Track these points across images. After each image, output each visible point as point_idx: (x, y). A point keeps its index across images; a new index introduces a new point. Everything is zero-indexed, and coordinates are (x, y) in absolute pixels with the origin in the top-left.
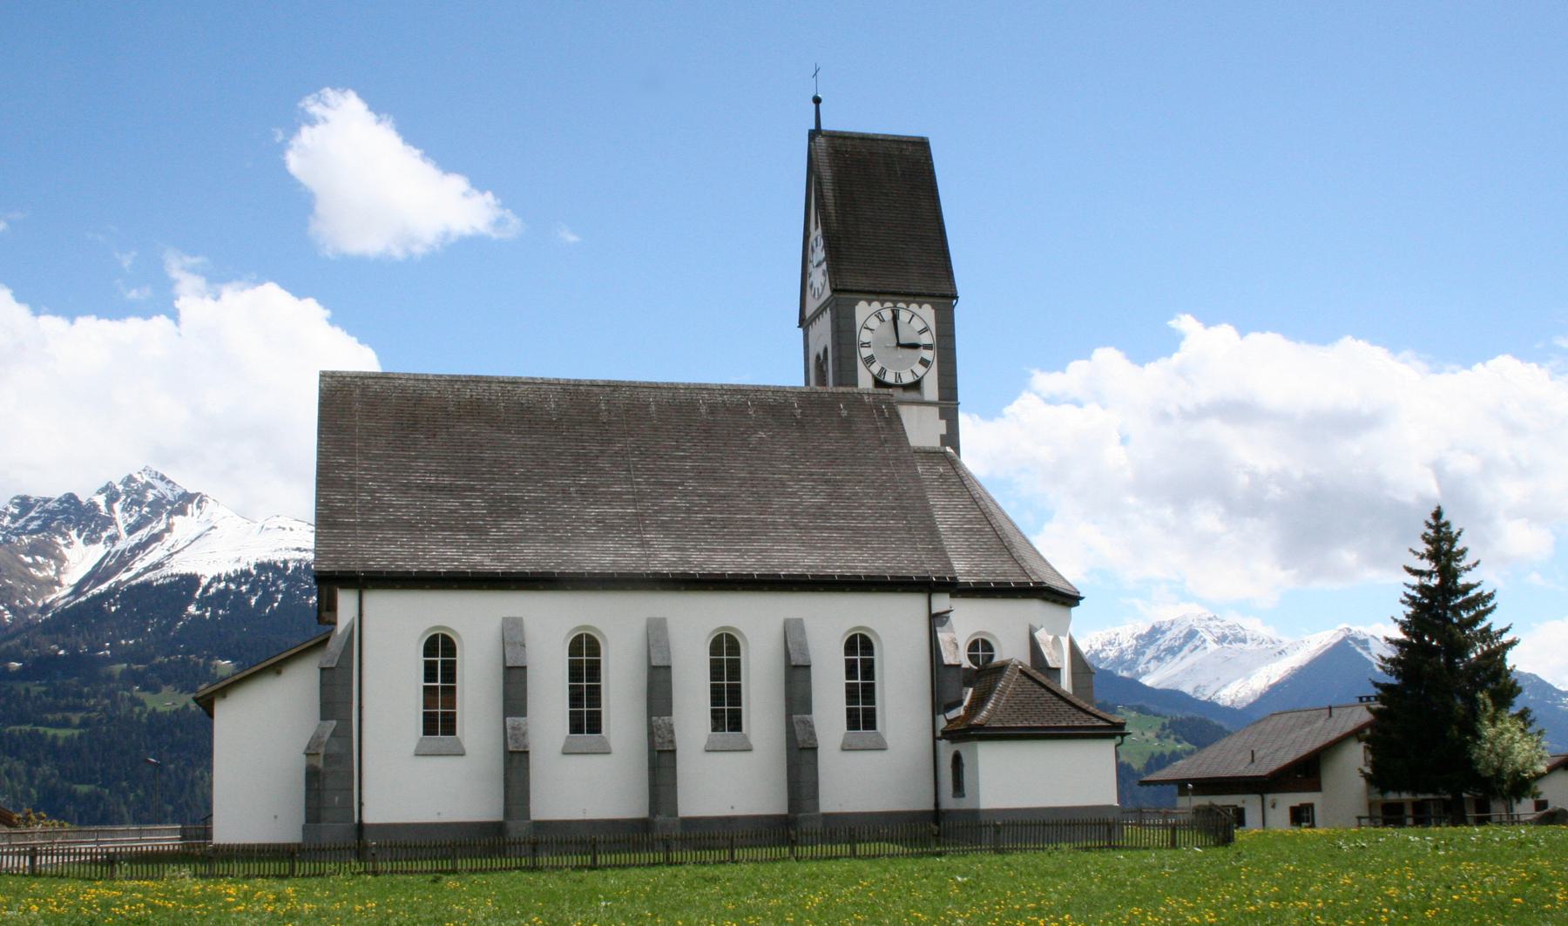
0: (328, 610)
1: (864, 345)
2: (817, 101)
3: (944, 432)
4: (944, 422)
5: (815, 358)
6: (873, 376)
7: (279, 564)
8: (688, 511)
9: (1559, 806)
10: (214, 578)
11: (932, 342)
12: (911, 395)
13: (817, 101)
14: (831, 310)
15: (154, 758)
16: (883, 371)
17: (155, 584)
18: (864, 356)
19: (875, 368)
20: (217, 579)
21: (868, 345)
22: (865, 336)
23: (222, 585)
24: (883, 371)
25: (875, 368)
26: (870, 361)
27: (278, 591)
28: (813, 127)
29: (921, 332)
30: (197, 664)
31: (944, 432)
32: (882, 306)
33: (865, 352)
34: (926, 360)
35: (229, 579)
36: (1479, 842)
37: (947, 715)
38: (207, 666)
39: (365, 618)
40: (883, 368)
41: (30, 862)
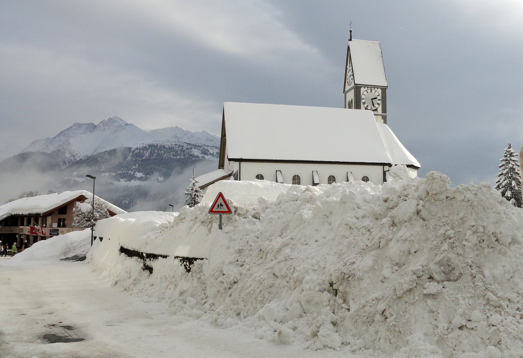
0: (222, 166)
2: (351, 31)
4: (383, 120)
5: (348, 101)
7: (155, 145)
10: (136, 149)
13: (351, 31)
14: (354, 89)
17: (118, 150)
18: (363, 102)
19: (366, 105)
20: (137, 149)
22: (363, 97)
23: (138, 151)
25: (366, 105)
26: (364, 103)
27: (155, 153)
29: (378, 96)
30: (131, 174)
33: (363, 101)
34: (378, 105)
35: (140, 149)
38: (134, 174)
39: (241, 170)
41: (61, 223)
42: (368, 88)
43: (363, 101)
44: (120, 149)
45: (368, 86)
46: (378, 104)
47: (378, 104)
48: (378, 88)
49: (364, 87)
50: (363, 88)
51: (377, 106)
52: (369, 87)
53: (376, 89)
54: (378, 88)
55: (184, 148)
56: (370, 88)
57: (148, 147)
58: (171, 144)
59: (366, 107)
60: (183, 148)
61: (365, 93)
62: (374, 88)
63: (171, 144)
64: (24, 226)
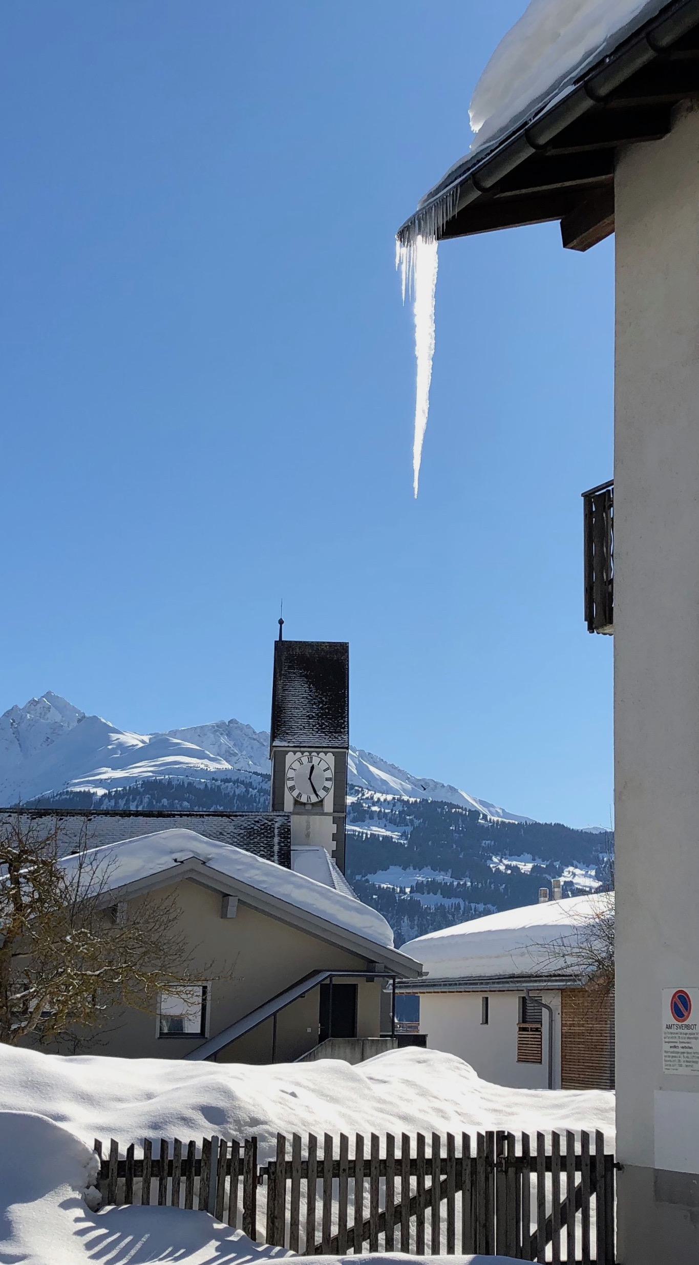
1: (289, 779)
2: (281, 622)
3: (553, 228)
6: (294, 797)
8: (70, 842)
9: (511, 973)
11: (331, 777)
12: (317, 809)
13: (281, 622)
15: (208, 1216)
16: (300, 795)
18: (289, 786)
19: (295, 793)
21: (292, 779)
22: (290, 774)
24: (300, 795)
25: (295, 793)
26: (292, 789)
28: (278, 640)
31: (553, 228)
32: (302, 754)
36: (613, 913)
37: (241, 1145)
40: (300, 793)
42: (303, 753)
43: (290, 784)
44: (57, 798)
45: (302, 749)
46: (326, 789)
47: (326, 789)
48: (326, 753)
49: (295, 753)
50: (291, 754)
51: (322, 793)
52: (314, 752)
53: (322, 755)
54: (326, 753)
55: (251, 790)
56: (307, 754)
57: (142, 790)
58: (213, 779)
59: (297, 797)
60: (247, 791)
61: (296, 765)
62: (318, 753)
63: (213, 779)
64: (426, 1047)
